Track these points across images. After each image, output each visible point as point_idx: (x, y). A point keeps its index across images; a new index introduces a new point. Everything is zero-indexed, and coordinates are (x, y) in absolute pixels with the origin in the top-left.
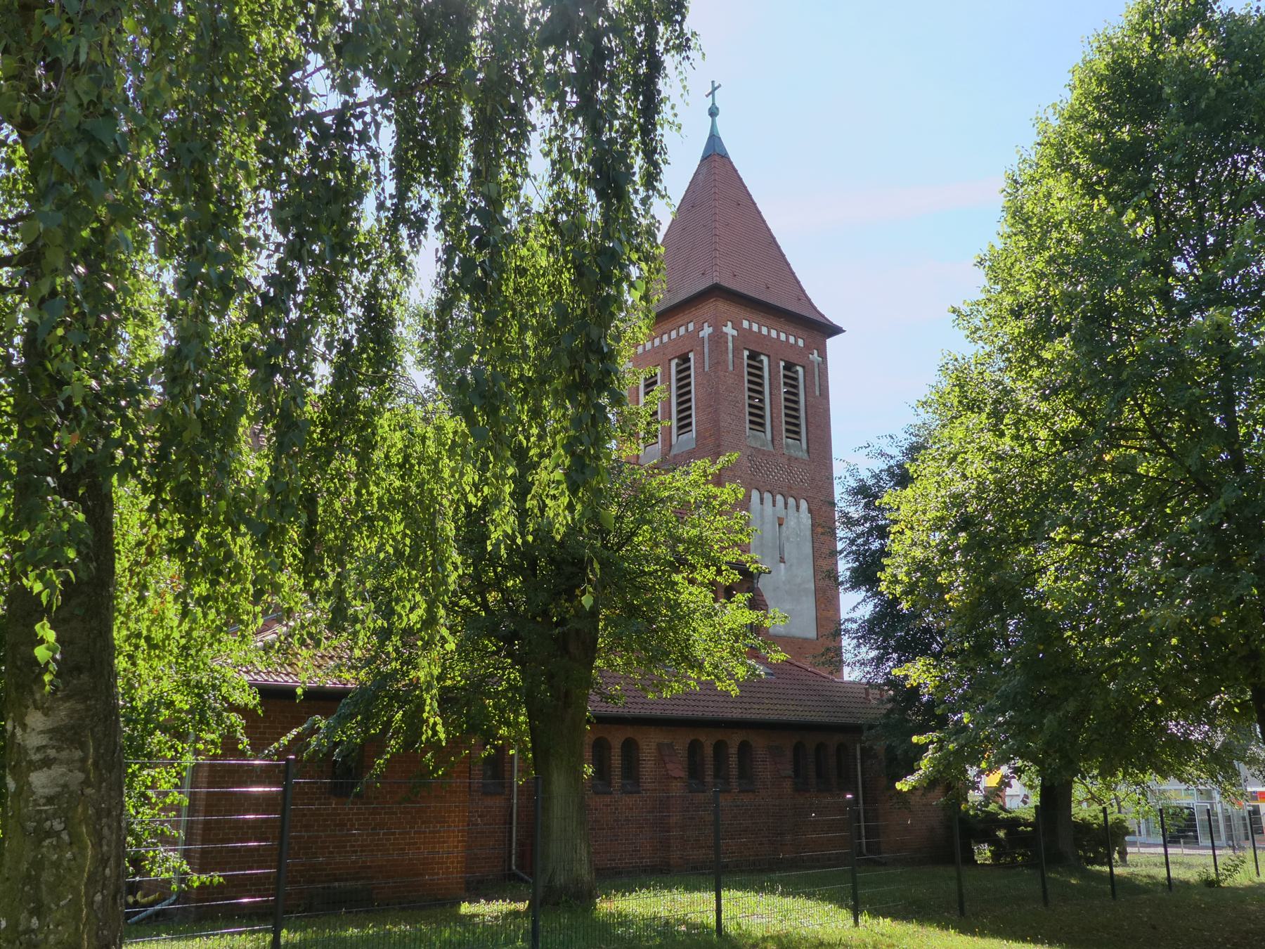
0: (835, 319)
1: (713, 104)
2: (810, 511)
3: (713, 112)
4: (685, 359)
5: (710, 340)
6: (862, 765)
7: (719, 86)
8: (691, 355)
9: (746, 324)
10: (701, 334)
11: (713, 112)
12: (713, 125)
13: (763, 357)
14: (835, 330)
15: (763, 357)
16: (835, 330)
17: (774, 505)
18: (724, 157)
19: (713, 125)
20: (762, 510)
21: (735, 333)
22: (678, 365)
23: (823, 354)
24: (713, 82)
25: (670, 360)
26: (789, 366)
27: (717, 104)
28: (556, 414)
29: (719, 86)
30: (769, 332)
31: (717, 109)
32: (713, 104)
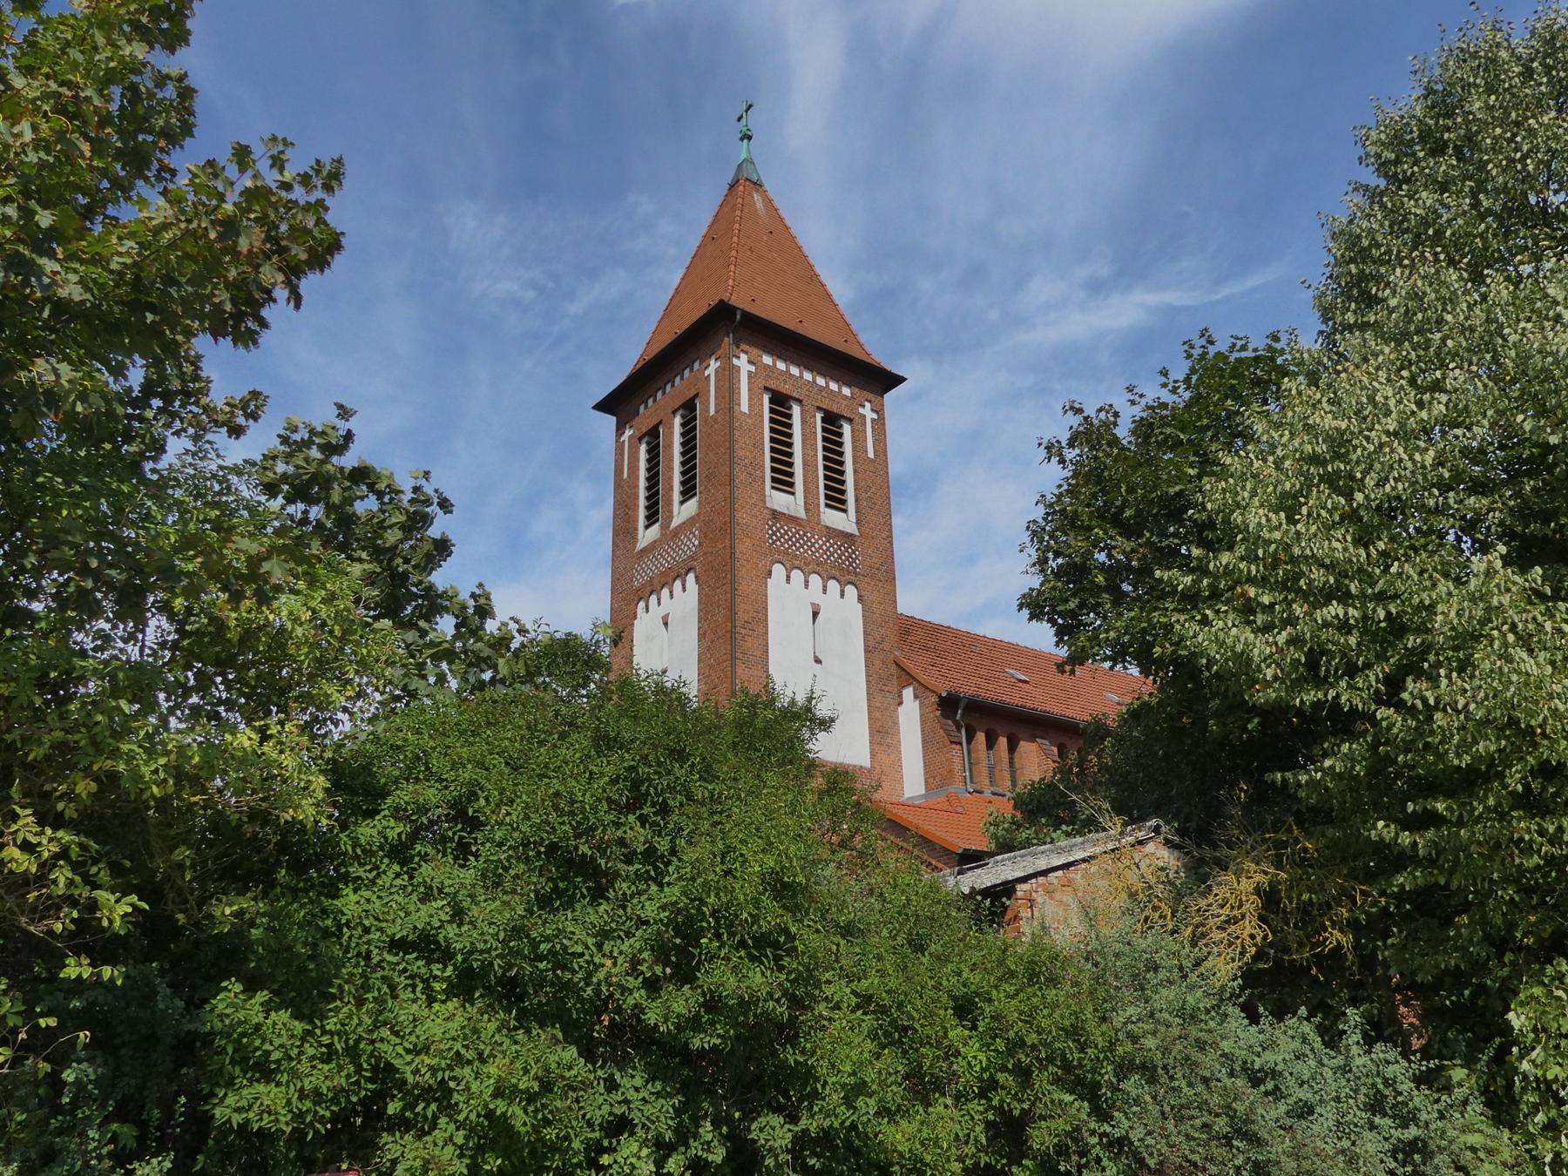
2: (860, 599)
9: (767, 360)
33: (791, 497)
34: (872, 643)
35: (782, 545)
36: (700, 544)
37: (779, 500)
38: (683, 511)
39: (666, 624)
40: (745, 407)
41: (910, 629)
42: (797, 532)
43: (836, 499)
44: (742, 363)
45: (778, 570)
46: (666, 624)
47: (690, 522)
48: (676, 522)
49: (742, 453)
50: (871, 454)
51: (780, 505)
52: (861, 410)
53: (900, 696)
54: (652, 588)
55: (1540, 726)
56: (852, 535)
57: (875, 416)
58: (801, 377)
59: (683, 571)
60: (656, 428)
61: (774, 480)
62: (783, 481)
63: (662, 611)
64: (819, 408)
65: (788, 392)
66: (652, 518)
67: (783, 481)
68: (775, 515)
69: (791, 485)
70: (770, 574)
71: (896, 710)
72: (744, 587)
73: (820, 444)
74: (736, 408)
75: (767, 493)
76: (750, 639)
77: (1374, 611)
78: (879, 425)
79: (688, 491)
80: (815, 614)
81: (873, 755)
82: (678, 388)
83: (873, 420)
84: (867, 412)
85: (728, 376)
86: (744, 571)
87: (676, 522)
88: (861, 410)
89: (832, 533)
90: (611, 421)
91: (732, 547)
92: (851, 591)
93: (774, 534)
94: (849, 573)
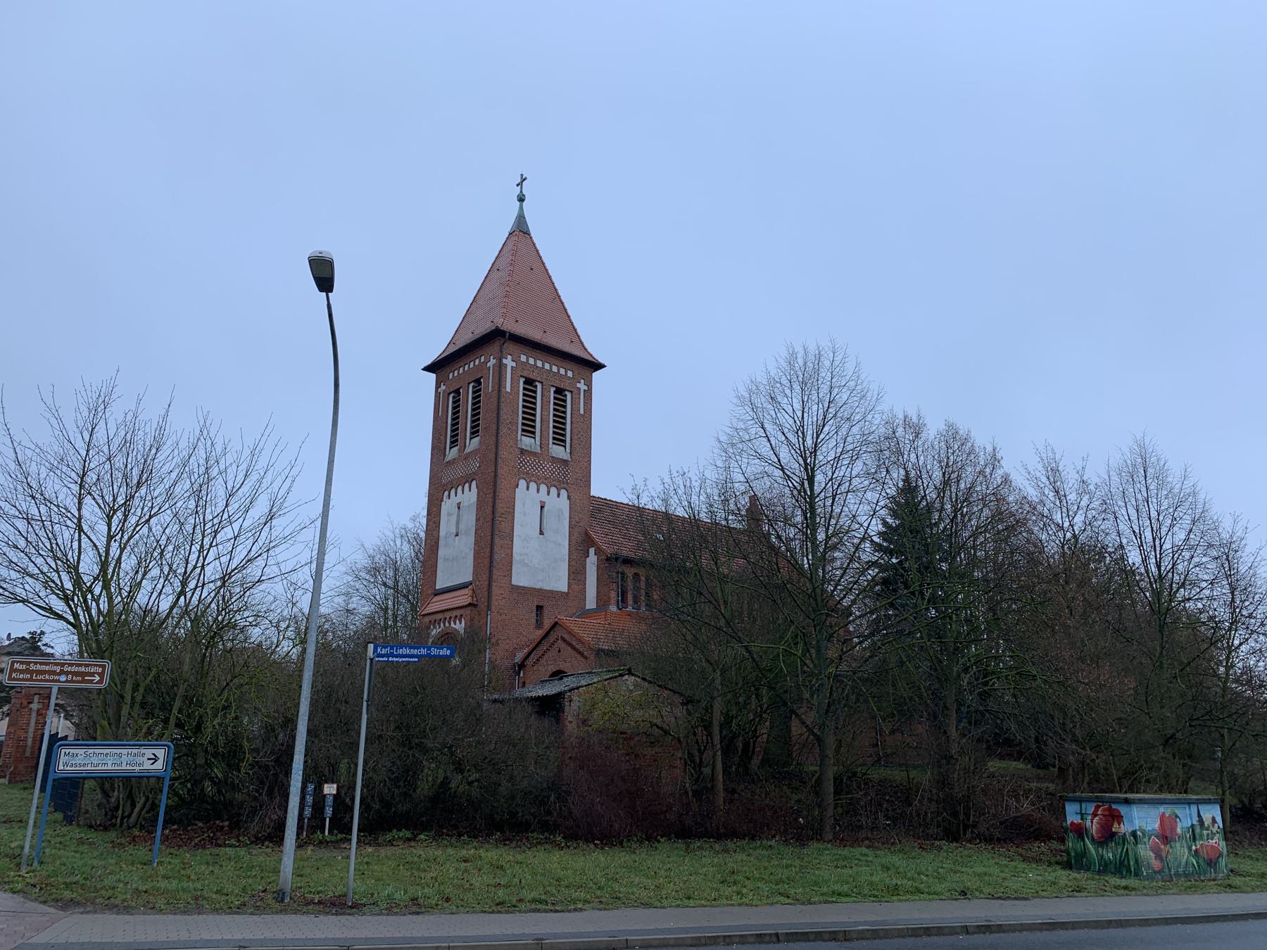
0: (601, 360)
1: (521, 192)
2: (569, 498)
3: (521, 199)
4: (478, 381)
5: (493, 367)
6: (749, 935)
7: (518, 185)
8: (482, 380)
9: (523, 358)
10: (489, 364)
11: (521, 199)
12: (521, 208)
13: (567, 393)
14: (598, 366)
15: (567, 393)
16: (598, 366)
18: (527, 233)
19: (521, 208)
21: (514, 364)
22: (474, 387)
23: (589, 384)
24: (522, 175)
25: (469, 384)
26: (559, 391)
27: (524, 193)
28: (340, 600)
29: (518, 185)
30: (566, 372)
31: (524, 195)
32: (521, 192)
33: (533, 440)
34: (573, 523)
35: (525, 468)
36: (480, 466)
37: (526, 442)
38: (473, 444)
39: (459, 508)
40: (508, 389)
41: (605, 508)
42: (535, 460)
43: (559, 439)
44: (509, 362)
45: (522, 483)
46: (459, 508)
47: (474, 452)
48: (468, 450)
49: (505, 417)
50: (582, 412)
51: (526, 445)
52: (578, 385)
53: (588, 552)
54: (453, 485)
55: (211, 743)
56: (567, 461)
57: (586, 388)
58: (543, 368)
59: (470, 480)
60: (459, 389)
61: (523, 430)
62: (529, 430)
63: (457, 500)
64: (552, 386)
65: (534, 378)
66: (454, 443)
67: (529, 430)
68: (523, 451)
69: (534, 433)
70: (517, 486)
71: (585, 561)
72: (503, 494)
73: (552, 406)
74: (503, 390)
75: (519, 438)
76: (503, 523)
77: (208, 786)
78: (588, 393)
79: (475, 433)
80: (542, 507)
81: (569, 586)
82: (473, 364)
83: (585, 390)
84: (582, 386)
85: (500, 367)
86: (503, 484)
87: (468, 450)
88: (578, 385)
89: (555, 460)
90: (433, 376)
91: (496, 472)
92: (564, 493)
93: (521, 462)
94: (564, 483)
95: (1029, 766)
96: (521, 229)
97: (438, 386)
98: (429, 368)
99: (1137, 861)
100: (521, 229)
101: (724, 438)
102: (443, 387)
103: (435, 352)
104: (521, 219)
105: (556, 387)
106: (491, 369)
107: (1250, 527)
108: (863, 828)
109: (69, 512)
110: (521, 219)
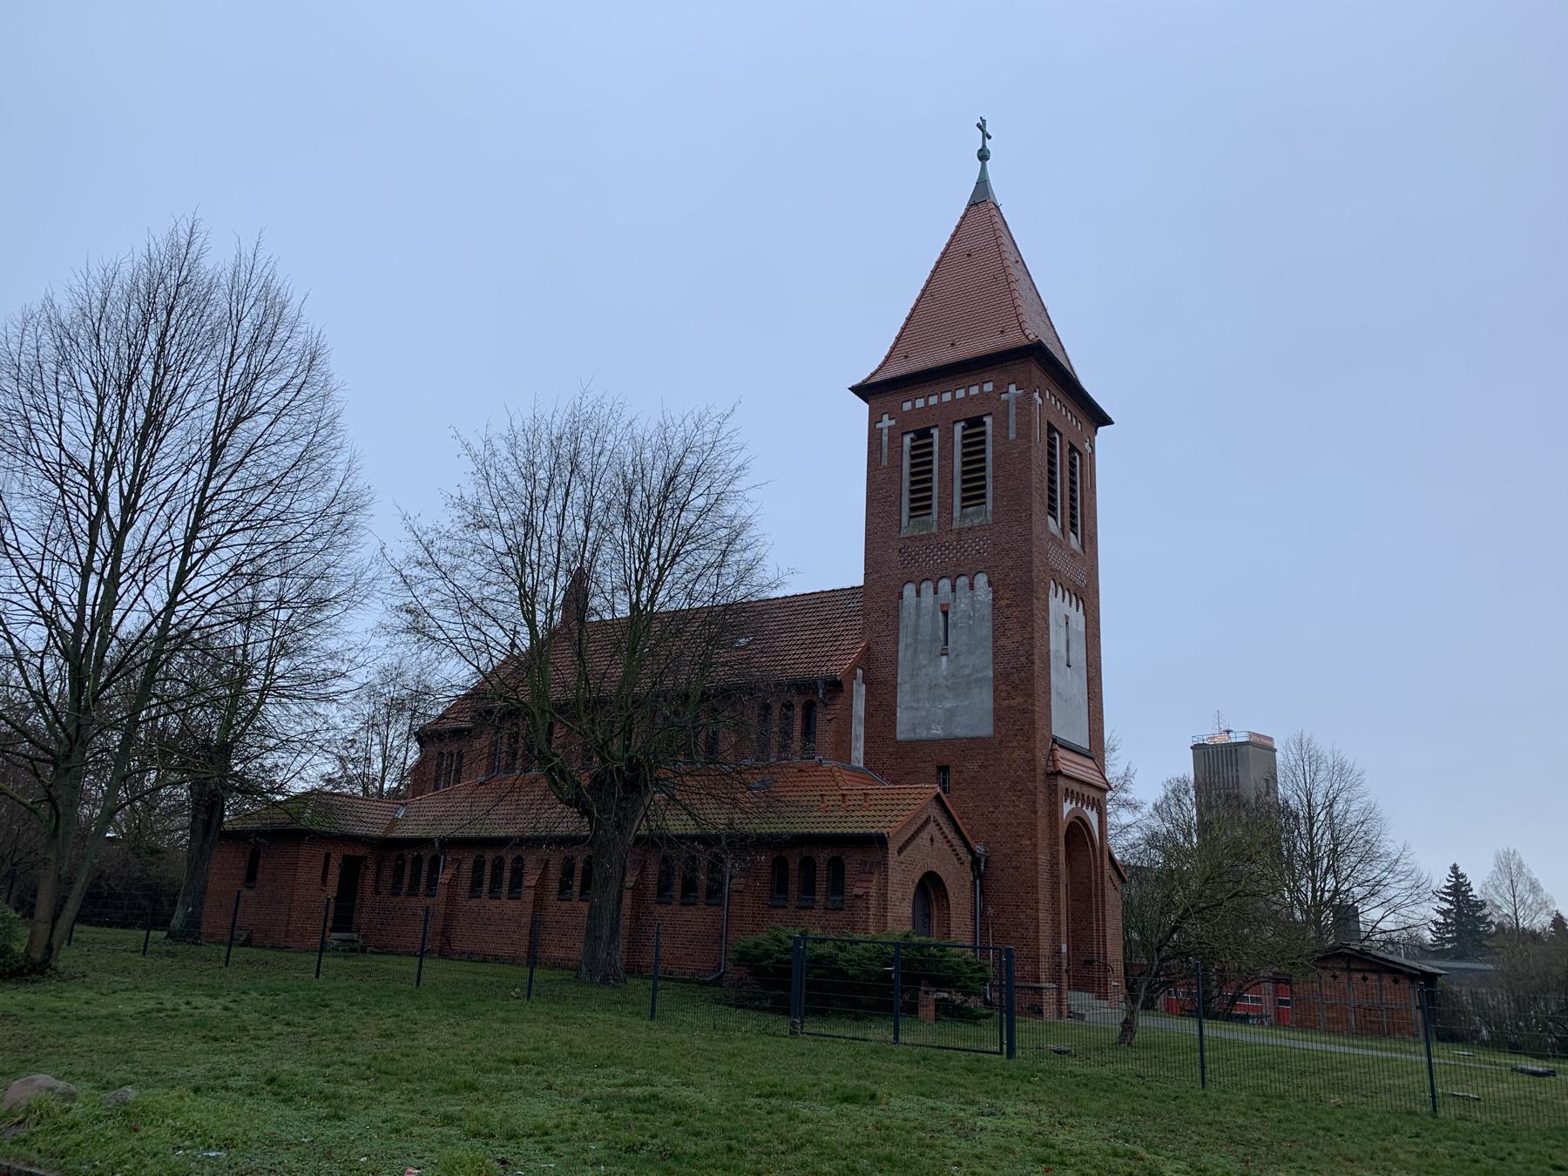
3: (983, 156)
11: (983, 156)
14: (1107, 421)
17: (936, 593)
20: (918, 604)
22: (964, 429)
95: (18, 916)
96: (982, 198)
97: (874, 420)
98: (862, 391)
99: (1336, 841)
100: (982, 198)
101: (518, 426)
102: (887, 422)
103: (867, 362)
104: (982, 185)
105: (966, 420)
106: (1013, 410)
107: (376, 499)
108: (806, 931)
109: (213, 626)
110: (982, 185)
